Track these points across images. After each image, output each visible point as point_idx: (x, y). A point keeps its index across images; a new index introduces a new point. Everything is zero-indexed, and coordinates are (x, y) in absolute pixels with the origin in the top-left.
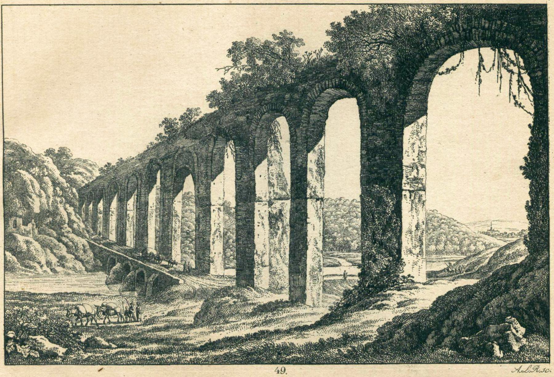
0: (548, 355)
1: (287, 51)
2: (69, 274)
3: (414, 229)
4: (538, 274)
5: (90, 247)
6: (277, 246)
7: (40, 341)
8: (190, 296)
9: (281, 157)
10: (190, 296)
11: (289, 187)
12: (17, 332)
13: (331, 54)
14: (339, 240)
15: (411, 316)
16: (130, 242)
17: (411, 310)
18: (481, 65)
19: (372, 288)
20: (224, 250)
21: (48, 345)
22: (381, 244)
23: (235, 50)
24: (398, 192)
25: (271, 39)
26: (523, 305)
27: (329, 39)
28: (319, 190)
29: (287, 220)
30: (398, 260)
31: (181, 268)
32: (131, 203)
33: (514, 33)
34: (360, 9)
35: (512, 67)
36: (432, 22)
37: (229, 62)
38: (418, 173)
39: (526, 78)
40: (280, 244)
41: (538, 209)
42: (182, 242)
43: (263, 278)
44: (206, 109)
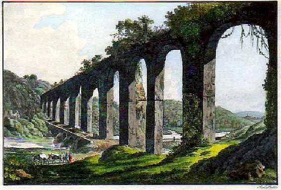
0: (277, 179)
1: (146, 26)
2: (35, 138)
3: (209, 115)
4: (271, 138)
5: (46, 125)
6: (140, 124)
7: (21, 172)
8: (97, 149)
9: (142, 79)
10: (97, 149)
11: (146, 95)
12: (9, 168)
13: (168, 27)
14: (171, 121)
15: (208, 160)
16: (66, 123)
17: (207, 157)
18: (243, 33)
19: (190, 144)
20: (114, 126)
21: (25, 175)
22: (192, 123)
23: (120, 26)
24: (201, 97)
25: (137, 20)
26: (263, 154)
27: (166, 20)
28: (161, 96)
29: (145, 112)
30: (201, 131)
31: (92, 135)
32: (67, 103)
33: (263, 17)
34: (182, 5)
35: (258, 34)
36: (218, 12)
37: (116, 31)
38: (211, 88)
39: (266, 40)
40: (141, 123)
41: (271, 106)
42: (93, 122)
43: (132, 140)
44: (105, 55)
